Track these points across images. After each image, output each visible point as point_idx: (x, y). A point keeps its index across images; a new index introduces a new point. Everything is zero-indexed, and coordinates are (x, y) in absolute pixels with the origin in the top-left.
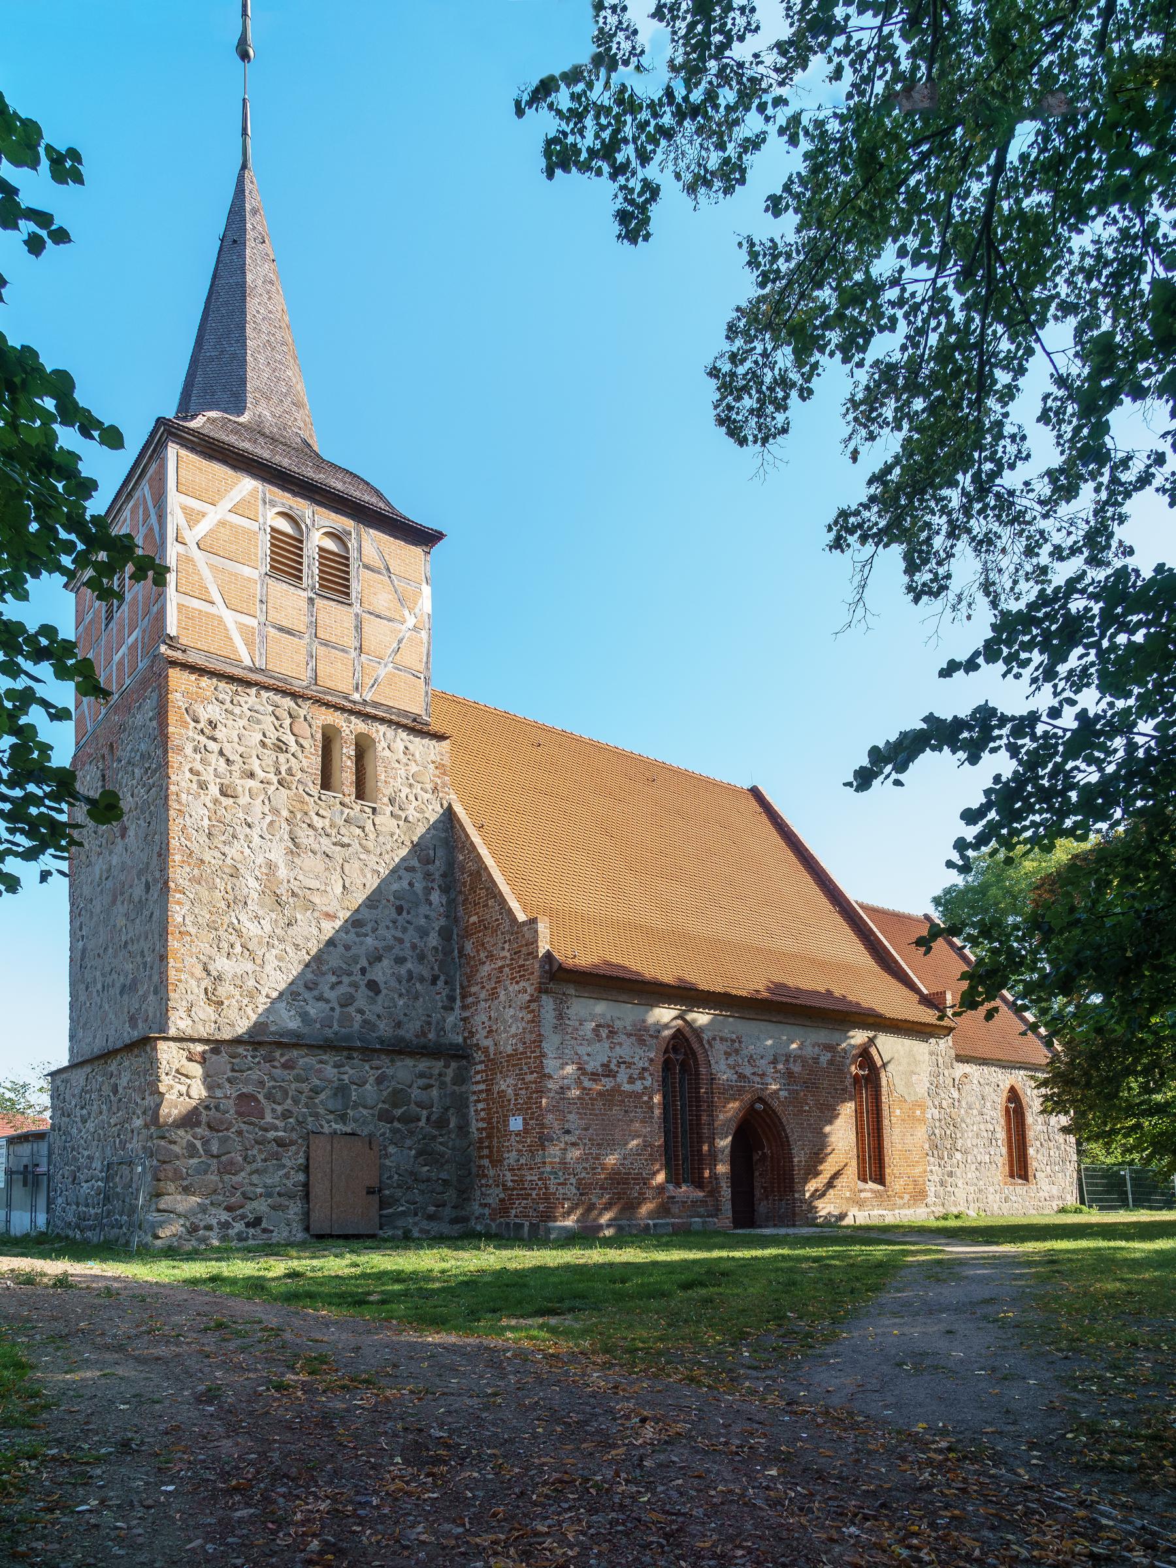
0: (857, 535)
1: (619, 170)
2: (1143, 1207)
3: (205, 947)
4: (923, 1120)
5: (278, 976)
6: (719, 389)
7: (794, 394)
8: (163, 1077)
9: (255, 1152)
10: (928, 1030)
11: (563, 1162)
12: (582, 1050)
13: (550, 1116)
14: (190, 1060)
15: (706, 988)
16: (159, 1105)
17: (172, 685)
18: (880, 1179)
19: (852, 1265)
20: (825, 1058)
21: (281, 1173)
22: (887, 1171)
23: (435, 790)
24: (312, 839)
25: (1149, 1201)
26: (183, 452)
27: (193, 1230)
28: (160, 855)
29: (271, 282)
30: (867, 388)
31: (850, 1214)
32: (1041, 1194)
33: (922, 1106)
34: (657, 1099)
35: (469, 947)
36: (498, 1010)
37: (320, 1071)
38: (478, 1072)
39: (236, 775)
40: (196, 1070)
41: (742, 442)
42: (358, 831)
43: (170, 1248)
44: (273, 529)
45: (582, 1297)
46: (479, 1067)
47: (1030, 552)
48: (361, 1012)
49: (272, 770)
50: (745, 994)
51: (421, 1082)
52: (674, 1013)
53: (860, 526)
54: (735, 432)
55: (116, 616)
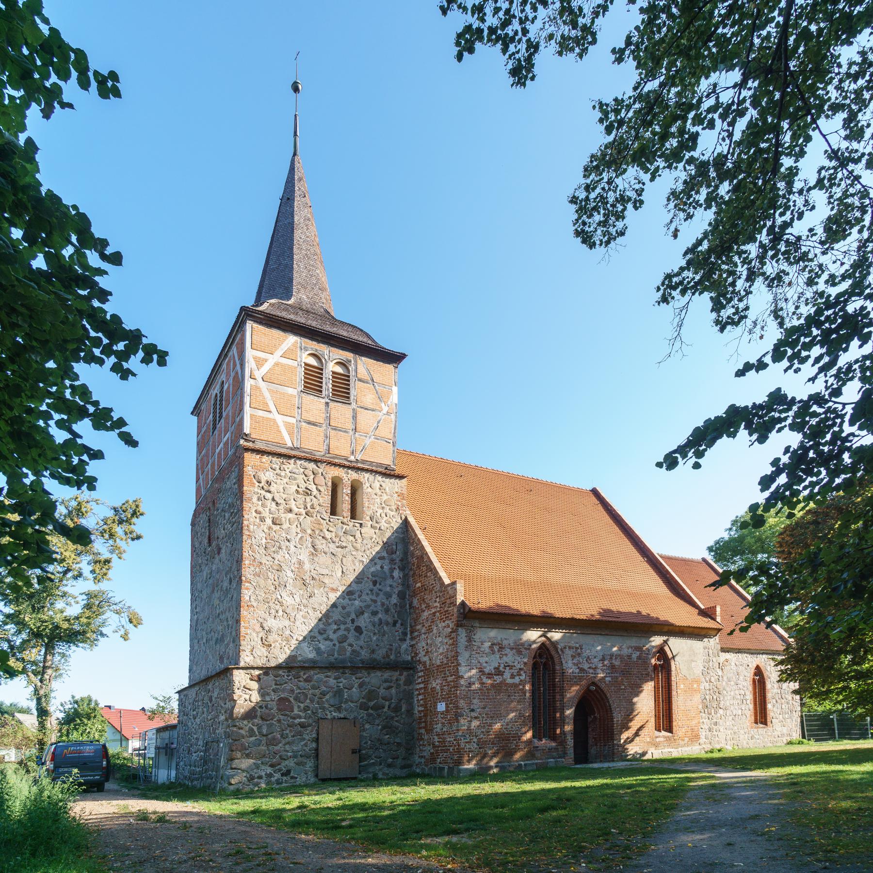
0: (678, 290)
1: (506, 42)
2: (846, 739)
3: (261, 613)
4: (699, 691)
5: (304, 625)
6: (577, 211)
7: (630, 206)
8: (236, 691)
9: (288, 732)
10: (703, 632)
11: (469, 729)
12: (483, 660)
13: (462, 701)
14: (251, 680)
15: (561, 616)
16: (233, 707)
17: (246, 462)
18: (670, 729)
19: (654, 790)
20: (635, 656)
21: (302, 743)
22: (674, 724)
23: (397, 509)
24: (324, 546)
25: (849, 734)
26: (255, 325)
27: (251, 779)
28: (237, 562)
29: (309, 220)
30: (685, 182)
31: (650, 753)
32: (776, 733)
33: (698, 682)
34: (527, 687)
35: (415, 602)
36: (432, 639)
37: (326, 682)
38: (419, 677)
39: (282, 511)
40: (255, 685)
41: (592, 246)
42: (352, 538)
43: (238, 790)
44: (306, 364)
45: (475, 820)
46: (420, 674)
47: (810, 282)
48: (351, 645)
49: (303, 506)
50: (585, 618)
51: (386, 685)
52: (540, 633)
53: (681, 283)
54: (586, 239)
55: (218, 426)
